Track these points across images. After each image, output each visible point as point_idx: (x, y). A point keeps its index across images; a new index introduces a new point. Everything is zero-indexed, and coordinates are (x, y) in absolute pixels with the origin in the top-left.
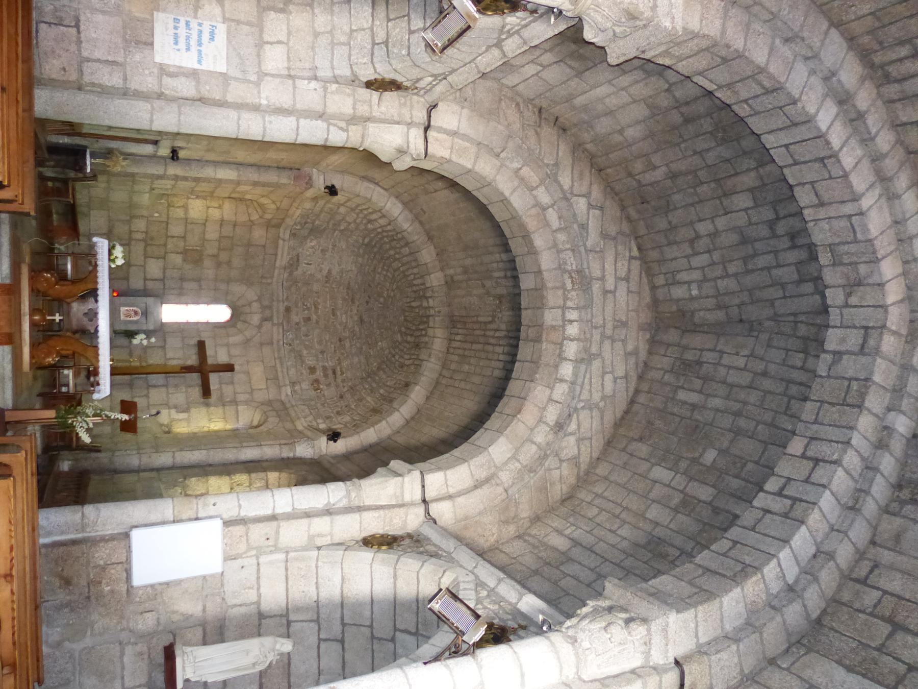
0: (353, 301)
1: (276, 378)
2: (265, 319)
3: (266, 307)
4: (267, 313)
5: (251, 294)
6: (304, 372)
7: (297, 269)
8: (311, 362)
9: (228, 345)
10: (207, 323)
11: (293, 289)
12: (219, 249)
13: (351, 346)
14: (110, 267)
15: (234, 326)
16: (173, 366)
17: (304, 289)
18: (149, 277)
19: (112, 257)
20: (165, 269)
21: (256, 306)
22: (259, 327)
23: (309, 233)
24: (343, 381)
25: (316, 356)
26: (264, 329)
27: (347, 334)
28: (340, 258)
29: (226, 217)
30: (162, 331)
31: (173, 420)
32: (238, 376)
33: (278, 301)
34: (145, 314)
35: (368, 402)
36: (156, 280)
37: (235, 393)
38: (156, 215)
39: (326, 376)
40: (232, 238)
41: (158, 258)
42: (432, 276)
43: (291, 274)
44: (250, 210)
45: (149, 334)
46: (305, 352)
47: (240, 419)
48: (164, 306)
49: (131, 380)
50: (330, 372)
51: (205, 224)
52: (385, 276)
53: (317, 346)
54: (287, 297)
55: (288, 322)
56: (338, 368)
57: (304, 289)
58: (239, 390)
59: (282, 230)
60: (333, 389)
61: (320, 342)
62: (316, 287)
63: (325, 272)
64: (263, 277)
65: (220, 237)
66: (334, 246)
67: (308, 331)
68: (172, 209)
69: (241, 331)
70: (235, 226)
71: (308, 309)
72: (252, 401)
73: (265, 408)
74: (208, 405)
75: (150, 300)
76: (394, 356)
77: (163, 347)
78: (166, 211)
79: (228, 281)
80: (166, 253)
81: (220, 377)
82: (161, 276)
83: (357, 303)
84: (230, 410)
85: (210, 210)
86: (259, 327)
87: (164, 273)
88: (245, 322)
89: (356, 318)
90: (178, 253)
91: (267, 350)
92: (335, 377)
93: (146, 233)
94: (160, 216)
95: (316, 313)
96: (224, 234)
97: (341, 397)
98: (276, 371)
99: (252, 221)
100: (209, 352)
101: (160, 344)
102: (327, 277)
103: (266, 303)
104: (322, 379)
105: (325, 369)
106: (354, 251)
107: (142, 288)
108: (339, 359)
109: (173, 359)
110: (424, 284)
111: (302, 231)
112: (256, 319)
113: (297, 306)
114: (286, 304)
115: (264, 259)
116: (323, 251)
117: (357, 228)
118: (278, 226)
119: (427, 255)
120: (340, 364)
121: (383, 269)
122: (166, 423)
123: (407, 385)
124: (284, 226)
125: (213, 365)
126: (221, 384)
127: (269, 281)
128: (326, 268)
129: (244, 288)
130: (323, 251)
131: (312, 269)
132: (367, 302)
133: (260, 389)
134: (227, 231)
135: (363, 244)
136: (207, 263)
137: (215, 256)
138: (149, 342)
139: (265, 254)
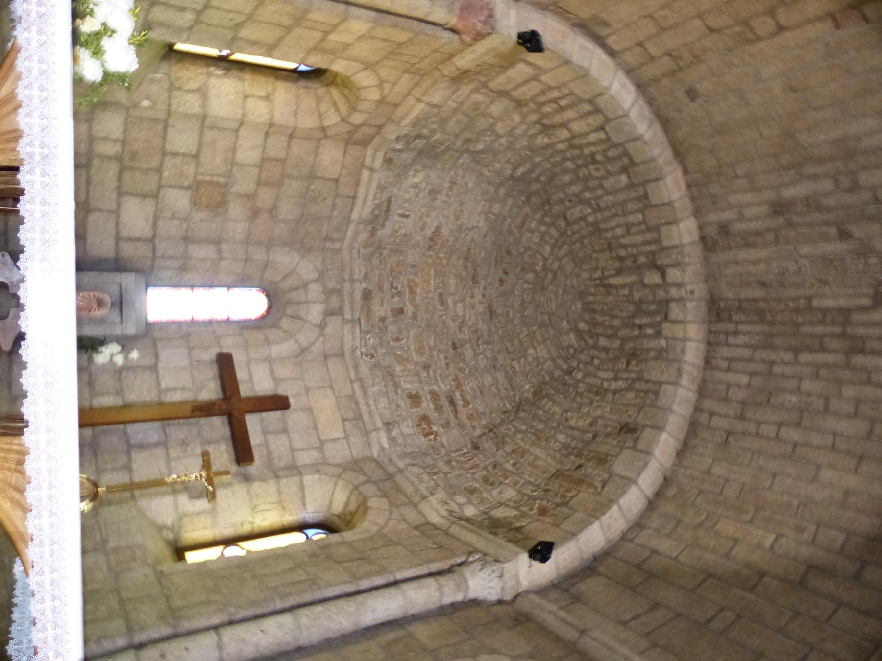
0: (475, 280)
1: (359, 417)
2: (329, 313)
3: (333, 291)
4: (334, 302)
5: (307, 268)
6: (401, 402)
7: (383, 225)
8: (410, 385)
9: (269, 360)
10: (228, 321)
11: (375, 261)
12: (259, 183)
13: (476, 355)
14: (78, 81)
15: (275, 325)
16: (174, 404)
17: (393, 260)
18: (125, 233)
19: (88, 26)
20: (156, 219)
21: (315, 290)
22: (322, 326)
23: (415, 159)
24: (470, 417)
25: (417, 374)
26: (329, 330)
27: (466, 335)
28: (461, 204)
29: (278, 119)
30: (151, 335)
31: (182, 517)
32: (294, 417)
33: (352, 280)
34: (120, 304)
35: (537, 458)
36: (138, 240)
37: (293, 450)
38: (146, 103)
39: (439, 408)
40: (283, 161)
41: (144, 196)
42: (682, 225)
43: (373, 234)
44: (323, 107)
45: (126, 343)
46: (398, 369)
47: (308, 500)
48: (151, 291)
49: (94, 437)
50: (445, 402)
51: (237, 131)
52: (543, 235)
53: (415, 357)
54: (366, 274)
55: (368, 316)
56: (457, 394)
57: (393, 260)
58: (298, 444)
59: (370, 151)
60: (455, 431)
61: (420, 350)
62: (412, 257)
63: (429, 232)
64: (327, 239)
65: (263, 160)
66: (453, 183)
67: (400, 332)
68: (176, 93)
69: (289, 335)
70: (291, 137)
71: (400, 294)
72: (326, 463)
73: (349, 475)
74: (247, 479)
75: (128, 280)
76: (569, 372)
77: (154, 368)
78: (164, 97)
79: (269, 245)
80: (160, 187)
81: (262, 420)
82: (148, 232)
83: (483, 283)
84: (290, 484)
85: (251, 104)
86: (322, 326)
87: (155, 225)
88: (297, 317)
89: (480, 308)
90: (182, 188)
91: (335, 367)
92: (456, 412)
93: (123, 142)
94: (153, 107)
95: (413, 300)
96: (272, 153)
97: (476, 447)
98: (357, 403)
99: (323, 129)
100: (241, 374)
101: (149, 361)
102: (431, 239)
103: (332, 285)
104: (434, 415)
105: (434, 395)
106: (487, 192)
107: (111, 254)
108: (456, 379)
109: (174, 389)
110: (657, 241)
111: (404, 155)
112: (315, 313)
113: (381, 289)
114: (364, 285)
115: (333, 207)
116: (433, 193)
117: (510, 147)
118: (364, 143)
119: (672, 186)
120: (458, 386)
121: (541, 222)
122: (169, 523)
123: (628, 429)
124: (376, 141)
125: (249, 399)
126: (265, 433)
127: (337, 245)
128: (432, 224)
129: (296, 257)
130: (433, 193)
131: (407, 226)
132: (501, 281)
133: (335, 440)
134: (277, 147)
135: (511, 176)
136: (236, 209)
137: (250, 197)
138: (126, 357)
139: (337, 196)
